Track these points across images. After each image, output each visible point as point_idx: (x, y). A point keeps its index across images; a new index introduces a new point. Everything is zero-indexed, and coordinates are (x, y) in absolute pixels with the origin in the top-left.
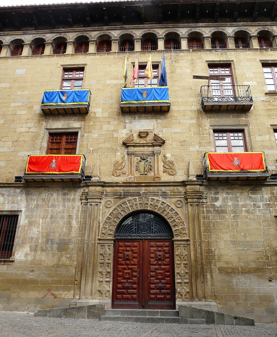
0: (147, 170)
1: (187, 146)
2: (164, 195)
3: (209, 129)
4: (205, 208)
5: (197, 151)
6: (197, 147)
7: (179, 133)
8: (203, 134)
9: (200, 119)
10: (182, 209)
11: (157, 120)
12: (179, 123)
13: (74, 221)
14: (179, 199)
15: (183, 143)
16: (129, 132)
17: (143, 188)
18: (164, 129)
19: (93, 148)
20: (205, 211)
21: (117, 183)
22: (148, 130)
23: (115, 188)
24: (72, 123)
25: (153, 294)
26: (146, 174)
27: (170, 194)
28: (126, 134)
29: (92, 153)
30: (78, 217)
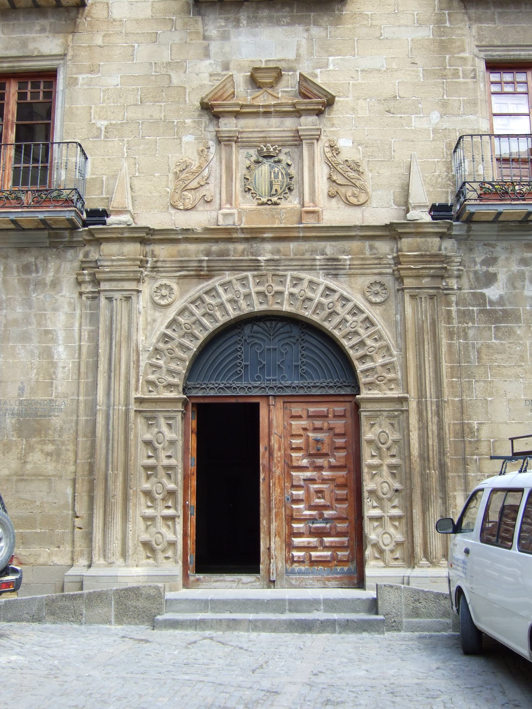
0: (279, 191)
1: (404, 113)
2: (333, 268)
3: (473, 60)
4: (454, 304)
5: (435, 131)
6: (435, 116)
7: (379, 71)
8: (456, 74)
9: (448, 24)
10: (385, 310)
11: (307, 30)
12: (378, 38)
13: (61, 349)
14: (378, 278)
15: (392, 104)
16: (219, 70)
17: (268, 246)
18: (331, 58)
19: (105, 123)
20: (454, 315)
21: (187, 230)
22: (279, 60)
23: (182, 247)
24: (34, 39)
25: (299, 548)
26: (276, 204)
27: (348, 263)
28: (211, 75)
29: (106, 137)
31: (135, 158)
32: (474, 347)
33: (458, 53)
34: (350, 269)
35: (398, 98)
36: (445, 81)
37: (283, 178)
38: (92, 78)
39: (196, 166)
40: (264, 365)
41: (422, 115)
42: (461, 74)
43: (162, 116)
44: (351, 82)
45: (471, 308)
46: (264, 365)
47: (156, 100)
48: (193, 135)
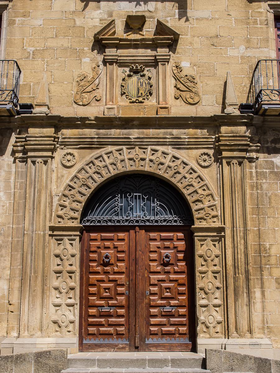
0: (144, 94)
3: (267, 14)
8: (255, 22)
15: (215, 40)
19: (33, 49)
26: (141, 102)
28: (101, 20)
29: (33, 58)
30: (10, 186)
31: (52, 72)
32: (266, 196)
33: (257, 9)
34: (188, 145)
35: (219, 36)
36: (248, 26)
37: (146, 86)
38: (24, 20)
39: (91, 77)
40: (133, 206)
41: (234, 48)
42: (258, 22)
43: (69, 45)
44: (189, 26)
45: (265, 170)
46: (133, 206)
47: (66, 35)
48: (88, 57)
